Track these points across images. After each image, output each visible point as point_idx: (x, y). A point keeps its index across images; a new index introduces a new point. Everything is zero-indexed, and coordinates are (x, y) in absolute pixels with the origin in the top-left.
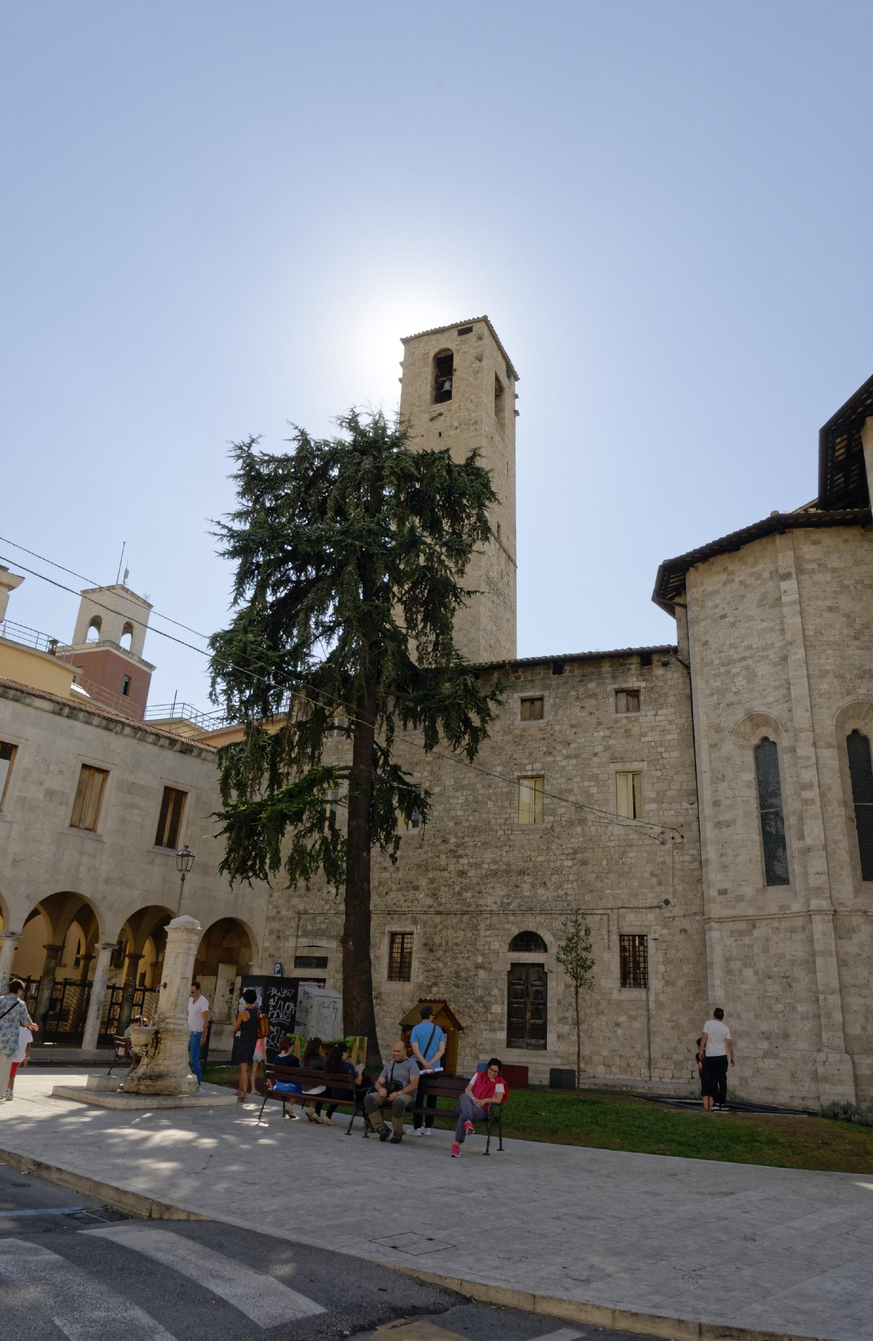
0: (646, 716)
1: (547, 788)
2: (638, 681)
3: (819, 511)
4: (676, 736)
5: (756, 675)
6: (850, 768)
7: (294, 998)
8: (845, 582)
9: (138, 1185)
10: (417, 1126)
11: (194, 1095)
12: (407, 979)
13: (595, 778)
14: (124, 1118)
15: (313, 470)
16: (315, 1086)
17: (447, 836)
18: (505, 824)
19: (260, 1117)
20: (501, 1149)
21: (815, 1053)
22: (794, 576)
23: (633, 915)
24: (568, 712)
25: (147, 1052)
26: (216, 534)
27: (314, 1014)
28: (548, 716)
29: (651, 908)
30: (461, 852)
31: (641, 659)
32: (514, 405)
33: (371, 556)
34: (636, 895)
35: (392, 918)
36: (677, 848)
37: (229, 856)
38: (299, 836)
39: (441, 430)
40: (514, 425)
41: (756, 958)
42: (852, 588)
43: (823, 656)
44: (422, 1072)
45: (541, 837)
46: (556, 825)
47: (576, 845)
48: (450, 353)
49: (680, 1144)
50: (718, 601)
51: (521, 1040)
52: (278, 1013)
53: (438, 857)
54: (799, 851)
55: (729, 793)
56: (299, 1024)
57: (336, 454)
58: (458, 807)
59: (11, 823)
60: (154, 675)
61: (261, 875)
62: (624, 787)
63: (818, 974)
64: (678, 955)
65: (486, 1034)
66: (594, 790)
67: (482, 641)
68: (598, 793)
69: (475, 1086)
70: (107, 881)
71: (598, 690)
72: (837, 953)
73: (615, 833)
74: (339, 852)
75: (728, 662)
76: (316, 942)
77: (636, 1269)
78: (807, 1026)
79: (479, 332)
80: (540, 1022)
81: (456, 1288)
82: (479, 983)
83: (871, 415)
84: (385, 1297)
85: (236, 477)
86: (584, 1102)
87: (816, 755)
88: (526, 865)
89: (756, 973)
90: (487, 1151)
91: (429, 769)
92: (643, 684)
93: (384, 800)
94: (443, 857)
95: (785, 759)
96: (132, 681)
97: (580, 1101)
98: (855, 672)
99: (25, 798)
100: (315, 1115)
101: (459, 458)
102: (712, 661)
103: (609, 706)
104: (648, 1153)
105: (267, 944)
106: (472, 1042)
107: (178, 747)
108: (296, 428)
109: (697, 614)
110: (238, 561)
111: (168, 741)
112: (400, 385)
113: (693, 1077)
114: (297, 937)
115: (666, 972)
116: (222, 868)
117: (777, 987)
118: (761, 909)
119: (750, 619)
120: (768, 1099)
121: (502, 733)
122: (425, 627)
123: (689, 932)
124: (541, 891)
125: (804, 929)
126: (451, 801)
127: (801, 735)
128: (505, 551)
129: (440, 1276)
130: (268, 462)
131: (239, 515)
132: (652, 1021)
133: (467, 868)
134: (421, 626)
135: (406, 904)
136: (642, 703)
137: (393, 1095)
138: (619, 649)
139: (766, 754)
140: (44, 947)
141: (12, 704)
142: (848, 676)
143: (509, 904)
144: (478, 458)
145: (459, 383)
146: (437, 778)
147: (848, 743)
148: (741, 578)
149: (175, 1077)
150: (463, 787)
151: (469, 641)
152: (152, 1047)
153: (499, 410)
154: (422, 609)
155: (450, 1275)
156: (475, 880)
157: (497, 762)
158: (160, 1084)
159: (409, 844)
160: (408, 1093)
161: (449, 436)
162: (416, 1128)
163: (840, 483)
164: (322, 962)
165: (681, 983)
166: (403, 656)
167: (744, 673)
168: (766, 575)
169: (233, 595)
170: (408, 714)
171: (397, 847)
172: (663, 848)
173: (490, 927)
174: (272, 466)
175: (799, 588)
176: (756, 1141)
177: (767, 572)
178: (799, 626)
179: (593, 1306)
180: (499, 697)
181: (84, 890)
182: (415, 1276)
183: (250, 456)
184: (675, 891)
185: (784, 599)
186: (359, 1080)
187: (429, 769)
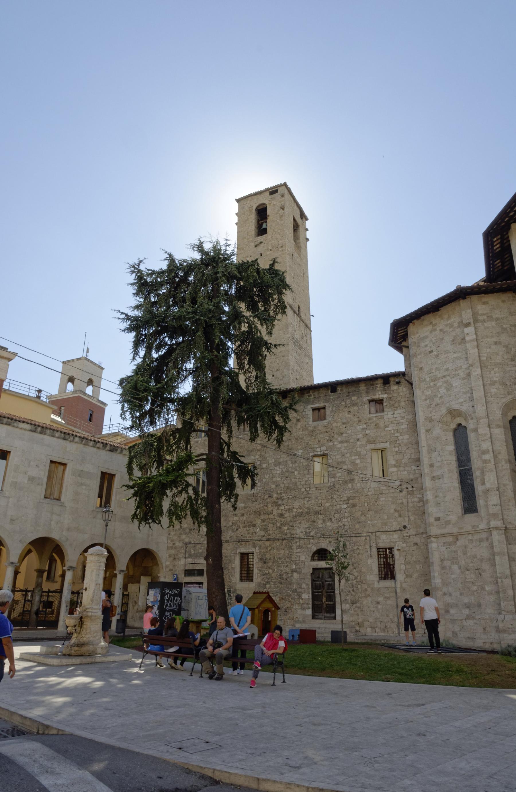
0: (388, 415)
1: (330, 461)
2: (382, 394)
3: (486, 284)
4: (406, 426)
5: (452, 386)
6: (512, 439)
7: (180, 595)
8: (505, 326)
9: (36, 713)
10: (235, 669)
11: (104, 655)
12: (252, 580)
13: (358, 454)
14: (53, 670)
15: (178, 277)
16: (171, 647)
17: (272, 494)
18: (306, 484)
19: (140, 667)
20: (284, 682)
21: (498, 615)
22: (472, 324)
23: (385, 536)
24: (341, 415)
25: (75, 630)
26: (119, 319)
27: (193, 605)
28: (329, 418)
29: (395, 531)
30: (280, 502)
31: (383, 381)
32: (306, 235)
33: (212, 325)
34: (386, 524)
35: (241, 544)
36: (410, 494)
37: (137, 511)
38: (174, 496)
39: (262, 252)
40: (306, 247)
41: (459, 559)
42: (509, 329)
43: (492, 372)
44: (236, 636)
45: (327, 491)
46: (336, 483)
47: (349, 495)
48: (265, 206)
49: (401, 674)
50: (427, 343)
51: (321, 614)
52: (170, 604)
53: (267, 506)
54: (483, 492)
55: (439, 459)
56: (184, 610)
57: (190, 267)
58: (277, 475)
59: (8, 498)
60: (107, 409)
61: (157, 521)
62: (376, 458)
63: (497, 567)
64: (413, 559)
65: (300, 612)
66: (358, 461)
67: (291, 376)
68: (361, 463)
69: (266, 643)
70: (68, 529)
71: (358, 401)
72: (508, 553)
73: (372, 486)
74: (199, 504)
75: (436, 379)
76: (196, 561)
77: (335, 758)
78: (492, 598)
79: (282, 192)
80: (331, 603)
81: (210, 775)
82: (294, 581)
83: (514, 222)
84: (160, 782)
85: (132, 284)
86: (346, 650)
87: (491, 433)
88: (319, 508)
89: (460, 568)
90: (274, 683)
91: (259, 453)
92: (385, 396)
93: (226, 474)
94: (269, 506)
95: (471, 436)
96: (94, 413)
97: (344, 650)
98: (512, 380)
99: (16, 482)
100: (173, 665)
101: (264, 265)
102: (425, 379)
103: (366, 411)
104: (379, 681)
105: (168, 563)
106: (292, 617)
107: (108, 448)
108: (166, 252)
109: (415, 351)
110: (133, 334)
111: (102, 445)
112: (236, 227)
113: (425, 633)
114: (186, 558)
115: (406, 569)
116: (133, 518)
117: (473, 576)
118: (461, 528)
119: (447, 352)
120: (469, 644)
121: (301, 430)
122: (249, 368)
123: (419, 544)
124: (329, 524)
125: (487, 539)
126: (273, 472)
127: (481, 421)
128: (303, 322)
129: (201, 767)
130: (151, 274)
131: (137, 307)
132: (399, 600)
133: (284, 512)
134: (247, 367)
135: (249, 536)
136: (385, 407)
137: (217, 651)
138: (370, 375)
139: (460, 433)
140: (35, 570)
141: (6, 427)
142: (508, 383)
143: (310, 532)
144: (276, 264)
145: (271, 224)
146: (264, 459)
147: (510, 425)
148: (441, 328)
149: (93, 645)
150: (280, 463)
151: (284, 377)
152: (79, 627)
153: (296, 238)
154: (247, 357)
155: (208, 766)
156: (289, 519)
157: (299, 447)
158: (84, 649)
159: (249, 499)
160: (226, 649)
161: (267, 255)
162: (234, 670)
163: (499, 266)
164: (200, 573)
165: (415, 575)
166: (237, 385)
167: (445, 385)
168: (456, 325)
169: (132, 355)
170: (241, 421)
171: (236, 501)
172: (401, 494)
173: (299, 547)
174: (154, 276)
175: (476, 331)
176: (449, 671)
177: (457, 323)
178: (477, 354)
179: (295, 785)
180: (294, 407)
181: (55, 535)
182: (186, 767)
183: (140, 271)
184: (409, 520)
185: (467, 338)
186: (197, 642)
187: (259, 453)
